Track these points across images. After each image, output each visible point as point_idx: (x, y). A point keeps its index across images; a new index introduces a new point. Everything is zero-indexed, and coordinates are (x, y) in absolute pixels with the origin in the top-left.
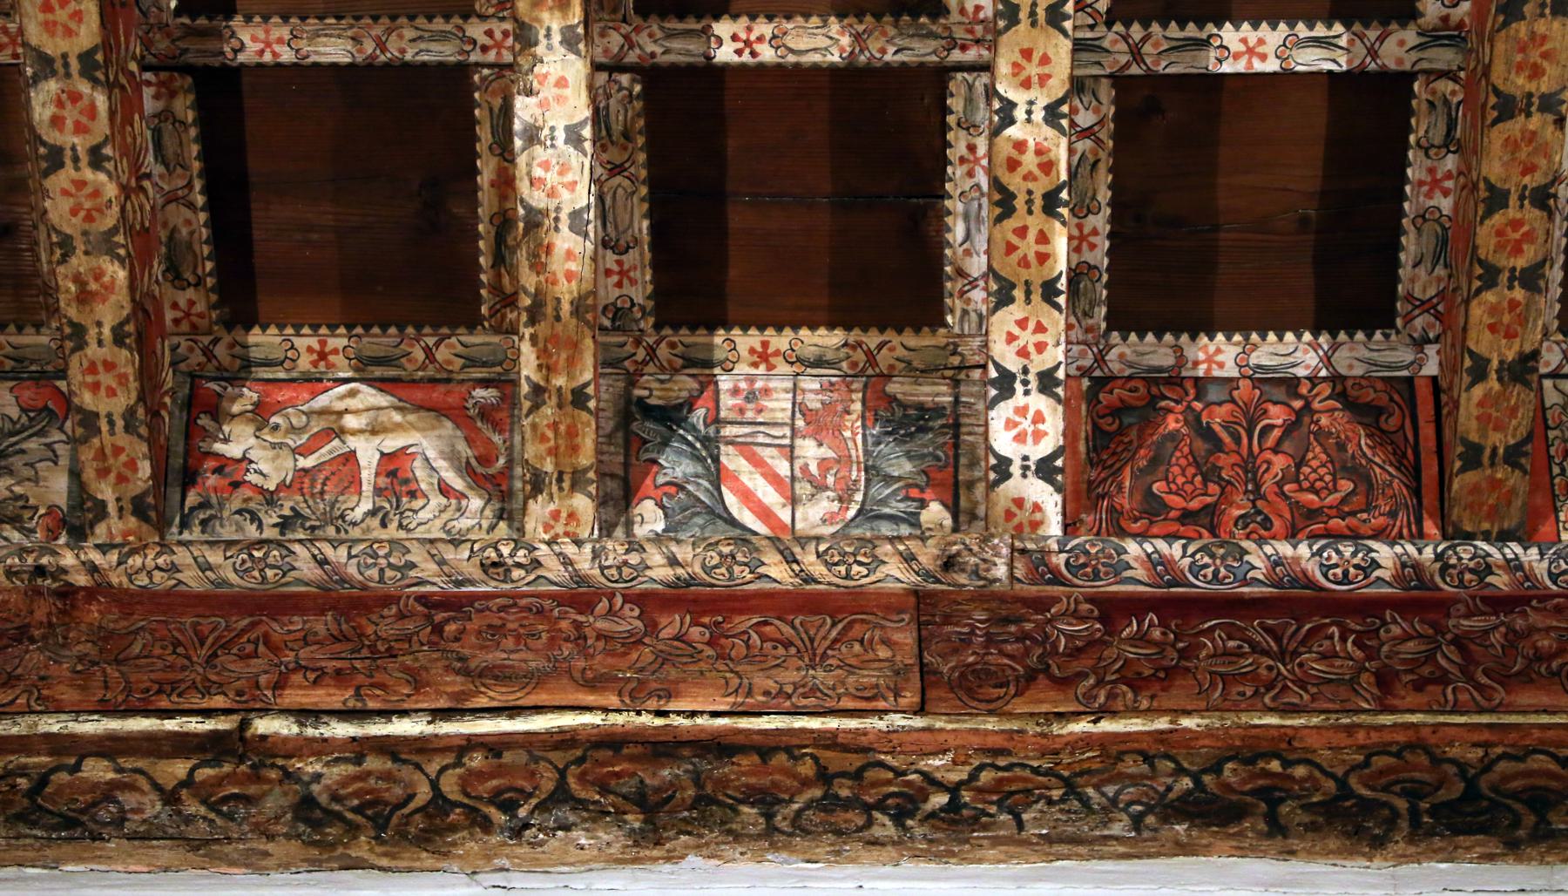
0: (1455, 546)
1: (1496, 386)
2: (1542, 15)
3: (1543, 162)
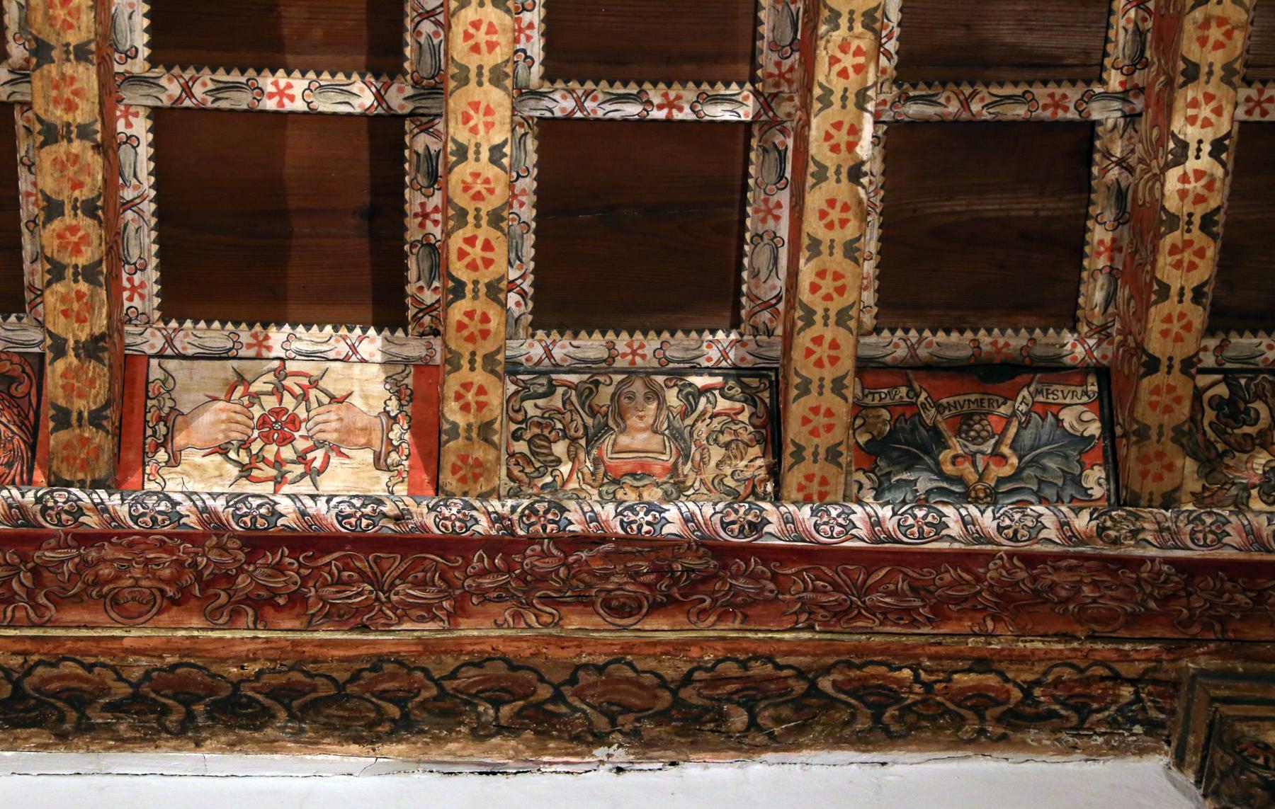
0: (53, 492)
1: (75, 361)
2: (68, 60)
3: (88, 180)
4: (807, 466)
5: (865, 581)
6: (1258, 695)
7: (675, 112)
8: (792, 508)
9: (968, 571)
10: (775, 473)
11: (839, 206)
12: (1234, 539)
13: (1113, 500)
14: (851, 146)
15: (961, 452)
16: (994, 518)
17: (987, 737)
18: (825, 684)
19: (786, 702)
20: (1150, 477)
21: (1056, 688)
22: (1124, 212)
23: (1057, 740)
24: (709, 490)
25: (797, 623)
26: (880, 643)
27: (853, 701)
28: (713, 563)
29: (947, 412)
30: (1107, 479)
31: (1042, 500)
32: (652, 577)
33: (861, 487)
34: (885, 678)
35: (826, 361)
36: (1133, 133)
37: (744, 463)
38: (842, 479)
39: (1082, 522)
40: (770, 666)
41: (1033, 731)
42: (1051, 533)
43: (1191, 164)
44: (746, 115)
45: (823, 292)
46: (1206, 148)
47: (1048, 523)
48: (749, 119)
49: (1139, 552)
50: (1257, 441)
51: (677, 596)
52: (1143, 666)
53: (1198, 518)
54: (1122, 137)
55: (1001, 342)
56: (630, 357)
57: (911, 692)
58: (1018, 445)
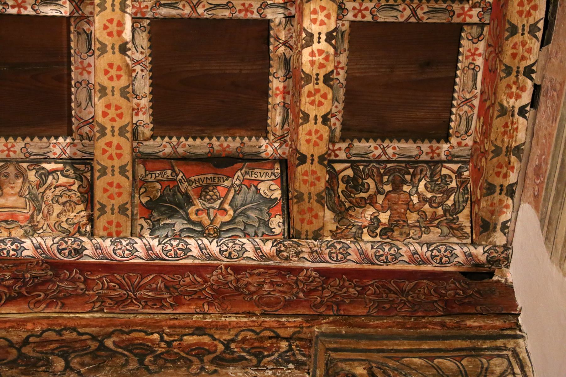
4: (108, 216)
5: (139, 282)
6: (353, 347)
7: (22, 10)
8: (100, 240)
9: (200, 276)
10: (91, 220)
11: (115, 67)
12: (353, 257)
13: (286, 235)
14: (120, 33)
15: (201, 208)
16: (218, 246)
17: (206, 372)
18: (109, 343)
19: (87, 354)
20: (306, 221)
21: (243, 343)
22: (289, 71)
23: (246, 373)
24: (52, 230)
25: (93, 308)
26: (141, 319)
27: (126, 353)
28: (50, 272)
29: (194, 185)
30: (284, 223)
31: (246, 235)
32: (11, 282)
33: (142, 228)
34: (143, 339)
35: (115, 156)
36: (291, 27)
37: (74, 214)
38: (129, 224)
39: (267, 248)
40: (75, 333)
41: (231, 368)
42: (250, 254)
43: (316, 46)
44: (66, 12)
45: (110, 117)
46: (323, 37)
47: (249, 249)
48: (68, 15)
49: (300, 264)
50: (368, 202)
51: (25, 293)
52: (292, 330)
53: (333, 245)
54: (284, 29)
55: (225, 145)
56: (6, 152)
57: (160, 347)
58: (234, 203)
